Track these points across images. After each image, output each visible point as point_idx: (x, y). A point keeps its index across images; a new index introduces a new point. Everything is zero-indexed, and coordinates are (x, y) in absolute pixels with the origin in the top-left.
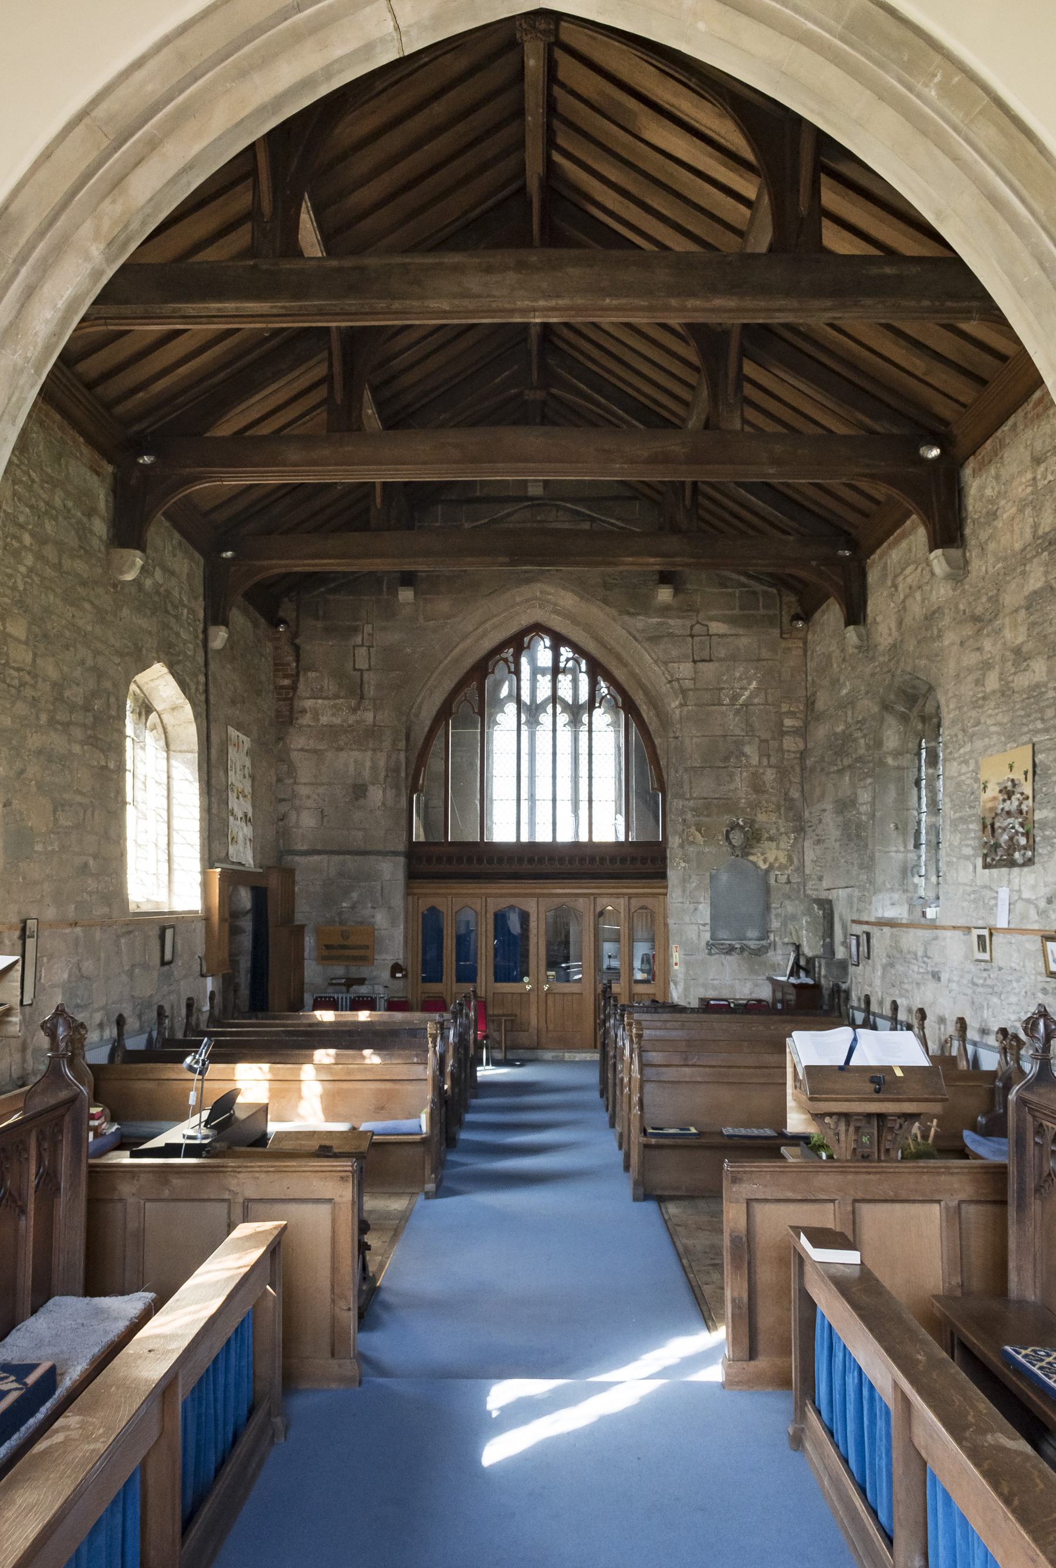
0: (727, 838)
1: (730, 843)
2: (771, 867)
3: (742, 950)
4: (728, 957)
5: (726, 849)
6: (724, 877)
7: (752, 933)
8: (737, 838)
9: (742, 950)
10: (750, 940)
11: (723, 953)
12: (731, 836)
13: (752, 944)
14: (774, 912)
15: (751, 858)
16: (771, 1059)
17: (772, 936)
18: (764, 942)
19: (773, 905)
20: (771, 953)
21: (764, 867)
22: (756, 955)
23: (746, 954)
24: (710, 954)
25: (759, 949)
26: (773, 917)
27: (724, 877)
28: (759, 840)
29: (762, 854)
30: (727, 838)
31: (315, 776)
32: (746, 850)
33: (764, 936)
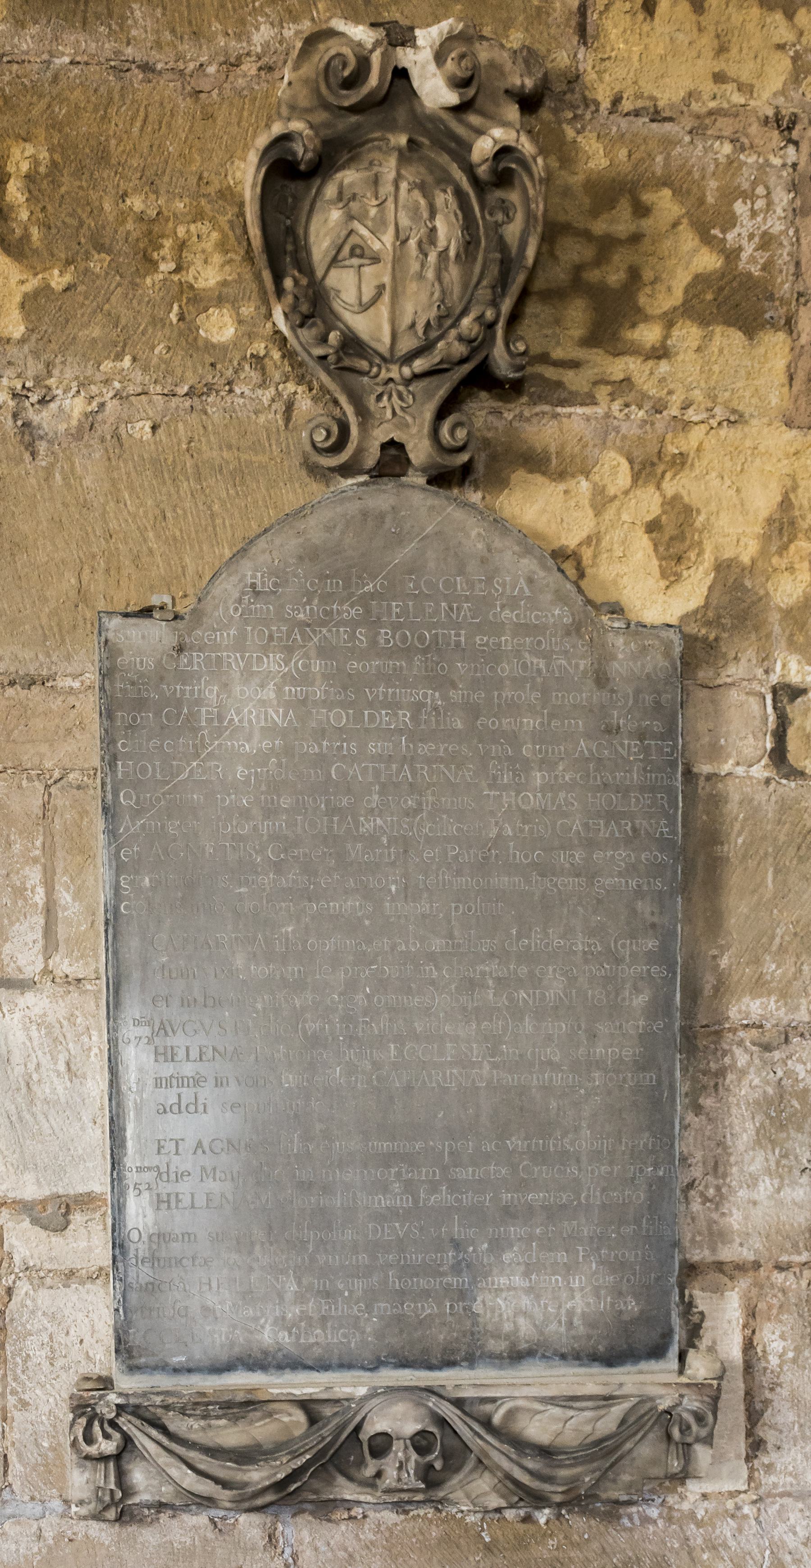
0: (281, 251)
1: (314, 307)
2: (736, 606)
3: (441, 1454)
4: (299, 1532)
5: (273, 407)
6: (252, 702)
7: (540, 1291)
8: (390, 254)
9: (441, 1454)
10: (517, 1356)
11: (249, 1501)
12: (324, 229)
13: (545, 1402)
14: (749, 1079)
15: (533, 504)
16: (430, 20)
17: (725, 1316)
18: (652, 1381)
19: (747, 1007)
20: (718, 1475)
21: (661, 602)
22: (577, 1501)
23: (474, 1493)
24: (120, 1508)
25: (605, 1451)
26: (743, 1128)
27: (252, 702)
28: (612, 317)
29: (647, 468)
30: (281, 251)
31: (634, 1459)
32: (483, 393)
33: (652, 1330)
